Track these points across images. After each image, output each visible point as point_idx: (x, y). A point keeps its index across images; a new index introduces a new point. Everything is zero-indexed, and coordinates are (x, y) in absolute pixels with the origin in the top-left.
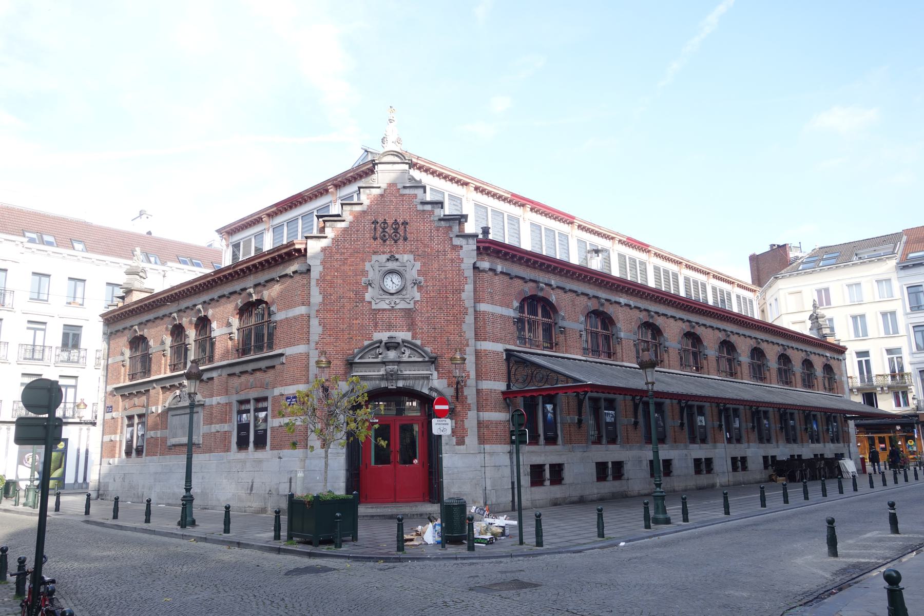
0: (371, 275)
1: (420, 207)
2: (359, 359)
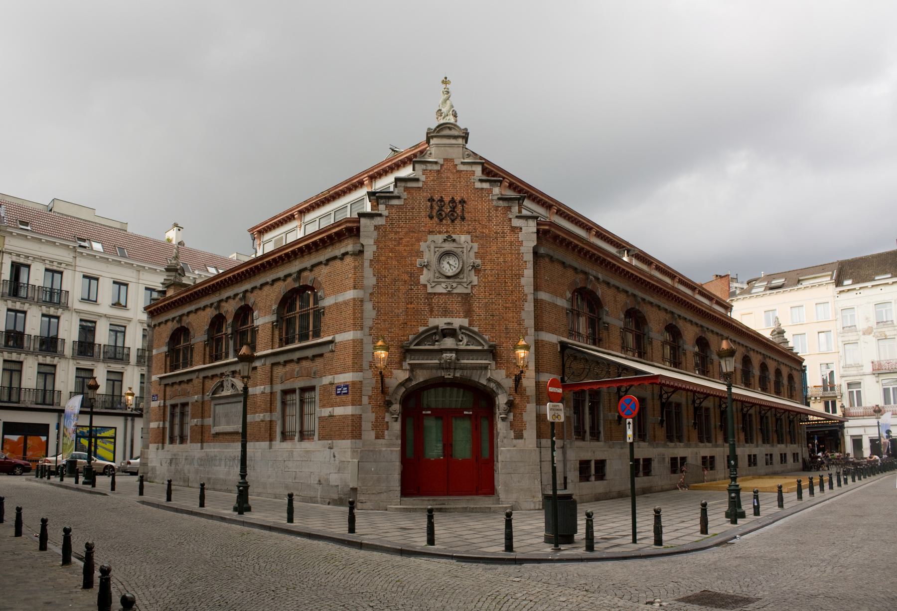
2: (416, 345)
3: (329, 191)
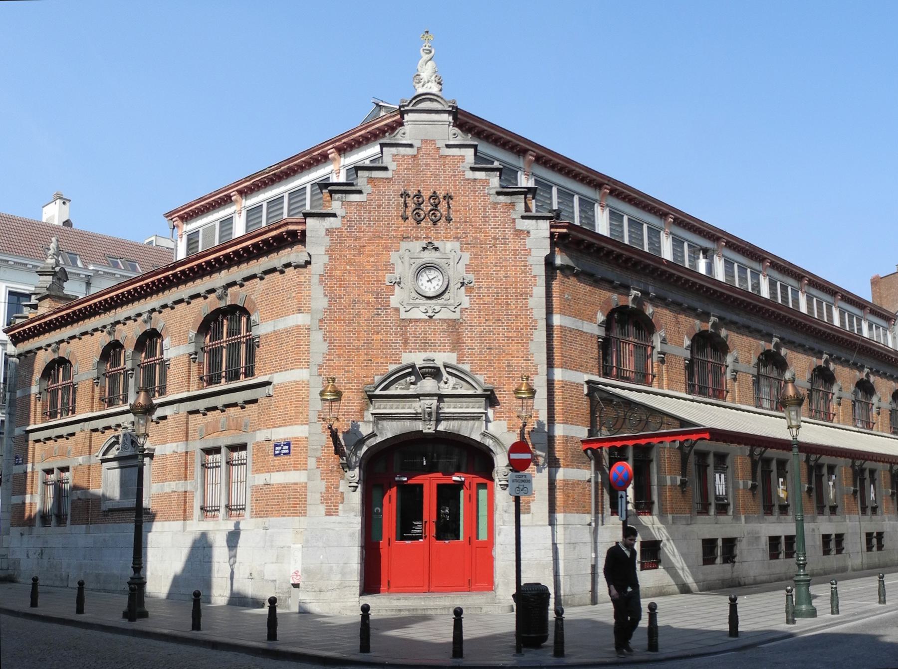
2: (384, 389)
3: (280, 165)
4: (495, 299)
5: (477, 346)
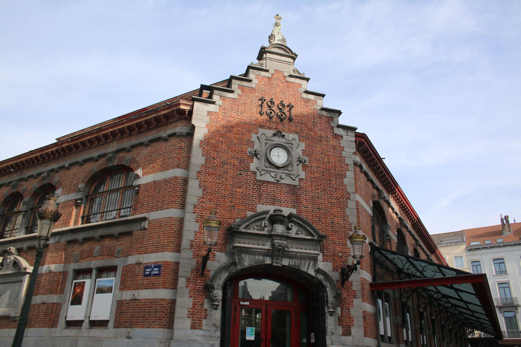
0: (257, 146)
1: (305, 96)
4: (322, 175)
5: (310, 206)
